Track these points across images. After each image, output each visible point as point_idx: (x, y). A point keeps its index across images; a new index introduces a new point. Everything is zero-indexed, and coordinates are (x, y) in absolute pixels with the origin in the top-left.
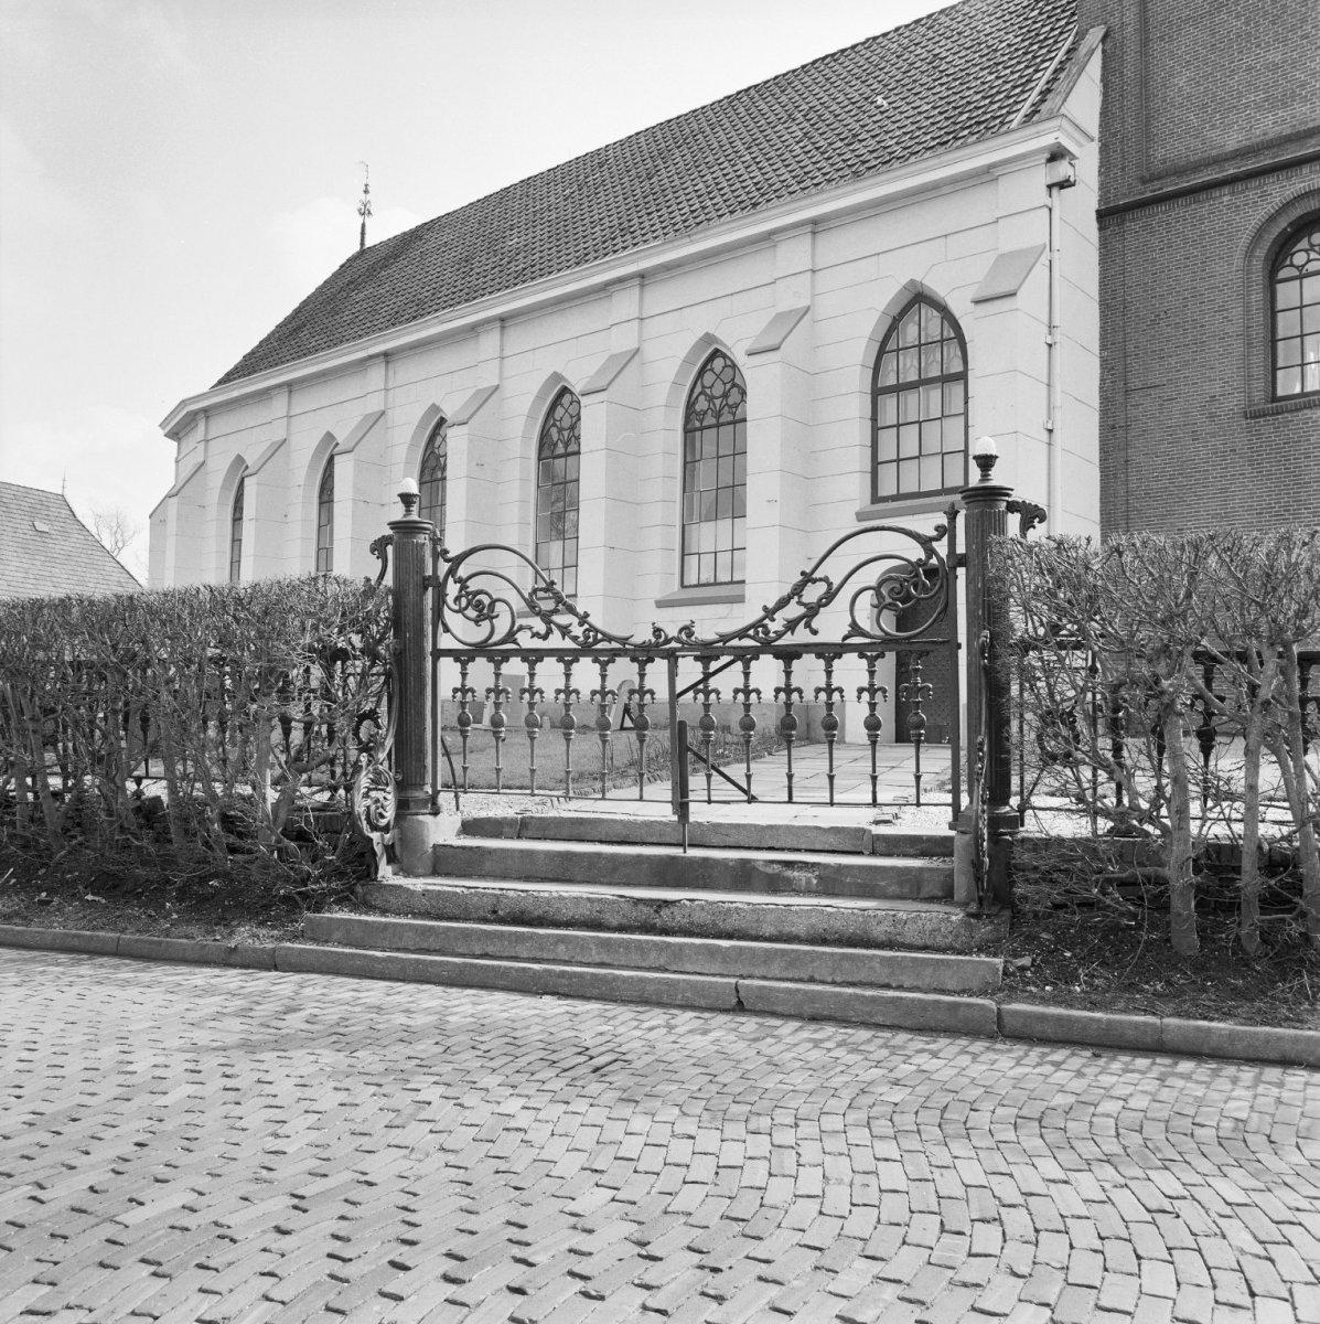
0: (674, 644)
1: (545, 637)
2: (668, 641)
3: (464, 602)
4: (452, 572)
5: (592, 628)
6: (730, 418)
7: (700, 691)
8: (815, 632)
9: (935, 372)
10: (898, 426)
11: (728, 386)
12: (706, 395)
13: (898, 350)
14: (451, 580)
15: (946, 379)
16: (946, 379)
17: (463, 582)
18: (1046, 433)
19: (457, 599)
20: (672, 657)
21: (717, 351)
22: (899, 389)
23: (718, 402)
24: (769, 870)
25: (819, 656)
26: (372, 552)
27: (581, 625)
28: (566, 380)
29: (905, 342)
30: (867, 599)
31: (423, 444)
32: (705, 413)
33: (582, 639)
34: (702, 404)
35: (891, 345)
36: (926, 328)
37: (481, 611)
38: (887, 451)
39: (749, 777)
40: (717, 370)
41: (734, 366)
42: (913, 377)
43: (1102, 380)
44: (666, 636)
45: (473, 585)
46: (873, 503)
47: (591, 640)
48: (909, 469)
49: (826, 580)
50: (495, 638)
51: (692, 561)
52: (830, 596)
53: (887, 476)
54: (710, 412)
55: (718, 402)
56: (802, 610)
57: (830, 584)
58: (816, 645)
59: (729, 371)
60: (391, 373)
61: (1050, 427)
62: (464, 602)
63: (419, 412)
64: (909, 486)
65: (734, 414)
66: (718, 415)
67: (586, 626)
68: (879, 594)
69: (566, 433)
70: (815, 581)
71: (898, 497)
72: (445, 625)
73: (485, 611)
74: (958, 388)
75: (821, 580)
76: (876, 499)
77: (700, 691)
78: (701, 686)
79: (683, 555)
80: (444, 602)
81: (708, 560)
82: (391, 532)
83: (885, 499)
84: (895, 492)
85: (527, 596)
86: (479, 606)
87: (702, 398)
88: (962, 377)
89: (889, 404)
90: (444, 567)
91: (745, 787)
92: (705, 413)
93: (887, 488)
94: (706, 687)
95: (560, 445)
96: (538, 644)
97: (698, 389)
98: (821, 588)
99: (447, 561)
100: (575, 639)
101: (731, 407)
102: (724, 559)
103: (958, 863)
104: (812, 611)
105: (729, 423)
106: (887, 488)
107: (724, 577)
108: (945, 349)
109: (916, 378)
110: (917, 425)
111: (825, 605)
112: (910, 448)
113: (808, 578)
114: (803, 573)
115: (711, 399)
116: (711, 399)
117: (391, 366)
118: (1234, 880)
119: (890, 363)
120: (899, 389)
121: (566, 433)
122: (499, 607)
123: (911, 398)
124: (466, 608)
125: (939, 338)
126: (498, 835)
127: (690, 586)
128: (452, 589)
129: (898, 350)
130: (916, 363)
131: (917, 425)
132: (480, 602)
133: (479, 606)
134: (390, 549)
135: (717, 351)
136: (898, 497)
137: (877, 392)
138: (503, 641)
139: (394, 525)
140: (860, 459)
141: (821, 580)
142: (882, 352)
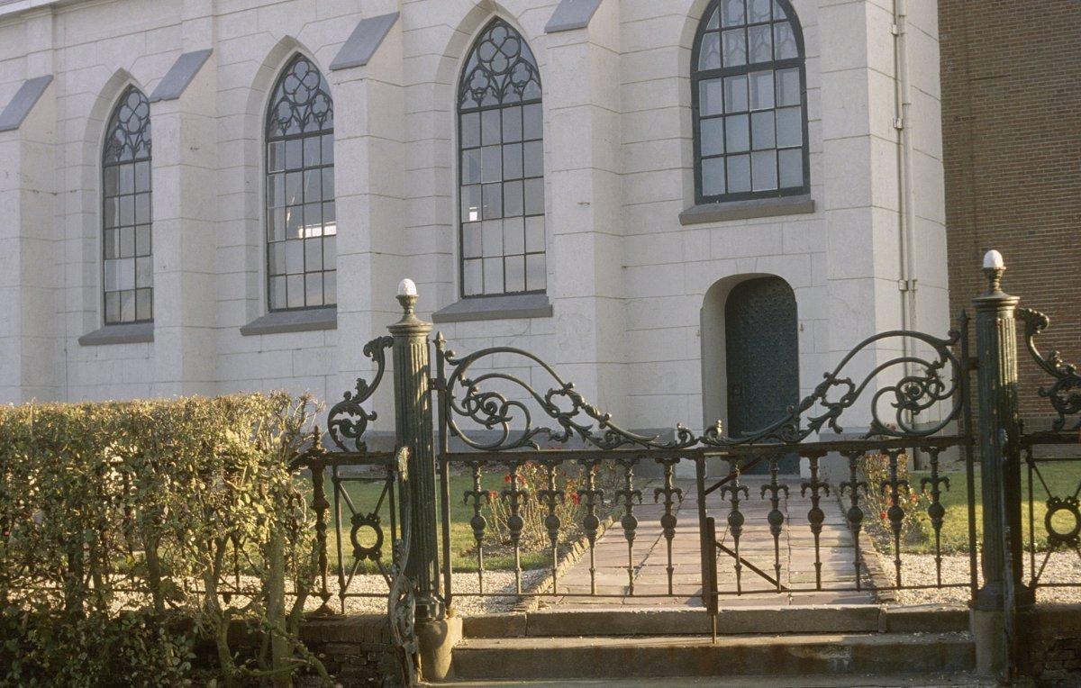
0: (700, 445)
1: (564, 439)
2: (694, 442)
3: (473, 404)
4: (457, 374)
5: (614, 430)
6: (517, 98)
7: (727, 488)
8: (839, 430)
9: (764, 56)
10: (724, 116)
11: (512, 61)
12: (485, 70)
13: (721, 30)
14: (457, 383)
15: (778, 65)
16: (778, 65)
17: (470, 384)
18: (895, 133)
19: (466, 402)
20: (698, 456)
21: (496, 18)
22: (724, 73)
23: (500, 79)
24: (801, 655)
25: (844, 453)
26: (367, 353)
27: (602, 426)
28: (299, 44)
29: (727, 22)
30: (891, 397)
31: (106, 118)
32: (484, 91)
33: (604, 440)
34: (479, 81)
35: (713, 24)
36: (751, 6)
37: (492, 414)
38: (712, 145)
39: (778, 567)
40: (498, 41)
41: (519, 37)
42: (738, 60)
43: (943, 66)
44: (692, 437)
45: (480, 389)
46: (697, 203)
47: (613, 441)
48: (739, 166)
49: (848, 381)
50: (505, 443)
51: (473, 268)
52: (852, 396)
53: (713, 170)
54: (489, 90)
55: (500, 79)
56: (826, 410)
57: (852, 386)
58: (841, 443)
59: (512, 44)
60: (60, 29)
61: (900, 126)
62: (473, 404)
63: (101, 78)
64: (740, 184)
65: (521, 94)
66: (500, 94)
67: (608, 428)
68: (899, 395)
69: (302, 110)
70: (837, 382)
71: (727, 197)
72: (452, 428)
73: (497, 414)
74: (792, 77)
75: (843, 382)
76: (700, 198)
77: (727, 488)
78: (728, 484)
79: (462, 259)
80: (452, 404)
81: (493, 266)
82: (391, 335)
83: (712, 199)
84: (723, 191)
85: (543, 397)
86: (490, 409)
87: (479, 73)
88: (798, 63)
89: (712, 89)
90: (449, 371)
91: (775, 578)
92: (484, 91)
93: (713, 187)
94: (734, 484)
95: (295, 123)
96: (557, 447)
97: (474, 62)
98: (844, 389)
99: (453, 363)
100: (597, 441)
101: (516, 86)
102: (515, 263)
103: (976, 635)
104: (836, 410)
105: (515, 104)
106: (713, 187)
107: (515, 285)
108: (775, 29)
109: (744, 63)
110: (746, 116)
111: (848, 405)
112: (739, 142)
113: (831, 380)
114: (826, 375)
115: (491, 75)
116: (491, 75)
117: (60, 20)
118: (289, 460)
119: (711, 45)
120: (724, 73)
121: (302, 110)
122: (512, 410)
123: (738, 84)
124: (476, 410)
125: (767, 19)
126: (504, 634)
127: (473, 297)
128: (459, 392)
129: (721, 30)
130: (742, 45)
131: (746, 116)
132: (492, 405)
133: (490, 409)
134: (388, 352)
135: (496, 18)
136: (727, 197)
137: (698, 77)
138: (519, 445)
139: (393, 329)
140: (677, 152)
141: (843, 382)
142: (701, 31)
